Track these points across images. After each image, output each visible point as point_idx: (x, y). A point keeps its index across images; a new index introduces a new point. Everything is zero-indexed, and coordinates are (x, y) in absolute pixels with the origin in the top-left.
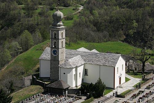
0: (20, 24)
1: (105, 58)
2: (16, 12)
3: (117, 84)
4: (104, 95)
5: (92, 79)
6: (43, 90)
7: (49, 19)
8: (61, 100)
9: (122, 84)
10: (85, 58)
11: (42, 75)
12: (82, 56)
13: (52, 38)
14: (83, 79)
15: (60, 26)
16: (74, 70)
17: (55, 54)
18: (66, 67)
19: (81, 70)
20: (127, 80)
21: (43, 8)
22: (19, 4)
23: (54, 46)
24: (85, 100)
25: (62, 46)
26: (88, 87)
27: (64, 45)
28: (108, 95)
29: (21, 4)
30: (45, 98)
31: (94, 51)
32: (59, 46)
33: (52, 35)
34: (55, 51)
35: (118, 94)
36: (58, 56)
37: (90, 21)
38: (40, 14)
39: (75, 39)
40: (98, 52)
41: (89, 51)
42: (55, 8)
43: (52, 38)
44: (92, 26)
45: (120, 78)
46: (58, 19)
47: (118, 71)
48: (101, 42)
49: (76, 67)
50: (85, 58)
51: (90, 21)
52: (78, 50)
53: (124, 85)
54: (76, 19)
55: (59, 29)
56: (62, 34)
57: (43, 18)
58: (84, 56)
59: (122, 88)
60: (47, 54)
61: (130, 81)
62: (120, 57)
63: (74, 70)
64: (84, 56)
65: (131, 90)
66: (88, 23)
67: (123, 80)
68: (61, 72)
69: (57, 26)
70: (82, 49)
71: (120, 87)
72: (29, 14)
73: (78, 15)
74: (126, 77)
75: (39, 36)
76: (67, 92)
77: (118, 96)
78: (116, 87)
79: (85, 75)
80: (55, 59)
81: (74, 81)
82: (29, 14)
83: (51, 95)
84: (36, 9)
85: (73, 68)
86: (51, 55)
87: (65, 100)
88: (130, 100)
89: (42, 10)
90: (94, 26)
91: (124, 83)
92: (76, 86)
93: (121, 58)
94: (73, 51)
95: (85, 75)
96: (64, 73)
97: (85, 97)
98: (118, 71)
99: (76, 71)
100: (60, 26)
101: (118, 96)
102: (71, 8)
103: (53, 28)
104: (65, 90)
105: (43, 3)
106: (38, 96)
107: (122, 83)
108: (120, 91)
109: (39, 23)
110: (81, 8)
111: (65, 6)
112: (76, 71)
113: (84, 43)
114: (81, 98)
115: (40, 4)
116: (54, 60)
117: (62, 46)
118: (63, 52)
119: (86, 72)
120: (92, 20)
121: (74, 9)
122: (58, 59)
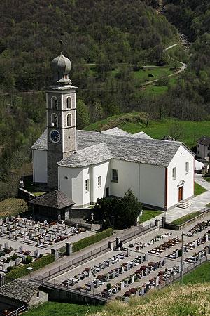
0: (86, 92)
1: (150, 149)
2: (81, 73)
3: (172, 199)
4: (140, 223)
5: (120, 191)
6: (24, 209)
7: (129, 84)
8: (47, 232)
9: (186, 200)
10: (114, 148)
11: (37, 180)
12: (109, 144)
13: (49, 109)
14: (107, 190)
15: (63, 84)
16: (85, 172)
17: (56, 140)
18: (68, 165)
19: (102, 171)
20: (198, 190)
21: (123, 67)
22: (88, 62)
23: (53, 124)
24: (98, 231)
25: (69, 124)
26: (106, 205)
27: (74, 123)
28: (146, 224)
29: (92, 62)
30: (21, 225)
31: (141, 135)
32: (61, 124)
33: (49, 103)
34: (57, 133)
35: (168, 221)
36: (61, 143)
37: (194, 88)
38: (118, 77)
39: (158, 114)
40: (149, 137)
41: (129, 135)
42: (142, 68)
43: (49, 109)
44: (197, 95)
45: (182, 188)
46: (61, 71)
47: (174, 175)
48: (201, 120)
49: (91, 166)
50: (114, 148)
51: (194, 88)
52: (104, 132)
53: (190, 202)
54: (173, 84)
55: (61, 90)
56: (69, 101)
57: (120, 83)
58: (114, 144)
59: (183, 207)
60: (42, 142)
61: (205, 193)
62: (181, 146)
63: (85, 172)
64: (114, 144)
65: (198, 213)
66: (191, 90)
67: (189, 191)
68: (62, 173)
69: (57, 85)
70: (116, 132)
71: (180, 206)
72: (100, 76)
73: (177, 78)
74: (195, 182)
75: (100, 109)
76: (67, 214)
77: (166, 226)
78: (168, 206)
79: (112, 181)
80: (55, 151)
81: (87, 190)
82: (100, 76)
83: (36, 220)
84: (113, 69)
85: (83, 168)
86: (49, 141)
87: (57, 232)
88: (187, 235)
89: (121, 71)
90: (201, 94)
91: (190, 198)
92: (91, 203)
93: (182, 149)
94: (94, 135)
95: (112, 181)
96: (67, 178)
97: (98, 227)
98: (174, 175)
99: (91, 172)
100: (63, 84)
101: (166, 226)
102: (167, 67)
103: (51, 89)
104: (63, 211)
105: (124, 61)
106: (10, 220)
107: (185, 197)
108: (172, 216)
109: (115, 90)
110: (183, 67)
111: (158, 64)
112: (91, 172)
113: (174, 121)
114: (89, 229)
115: (121, 62)
116: (54, 152)
117: (69, 124)
118: (71, 137)
119: (113, 175)
120: (197, 86)
121: (171, 69)
122: (61, 148)
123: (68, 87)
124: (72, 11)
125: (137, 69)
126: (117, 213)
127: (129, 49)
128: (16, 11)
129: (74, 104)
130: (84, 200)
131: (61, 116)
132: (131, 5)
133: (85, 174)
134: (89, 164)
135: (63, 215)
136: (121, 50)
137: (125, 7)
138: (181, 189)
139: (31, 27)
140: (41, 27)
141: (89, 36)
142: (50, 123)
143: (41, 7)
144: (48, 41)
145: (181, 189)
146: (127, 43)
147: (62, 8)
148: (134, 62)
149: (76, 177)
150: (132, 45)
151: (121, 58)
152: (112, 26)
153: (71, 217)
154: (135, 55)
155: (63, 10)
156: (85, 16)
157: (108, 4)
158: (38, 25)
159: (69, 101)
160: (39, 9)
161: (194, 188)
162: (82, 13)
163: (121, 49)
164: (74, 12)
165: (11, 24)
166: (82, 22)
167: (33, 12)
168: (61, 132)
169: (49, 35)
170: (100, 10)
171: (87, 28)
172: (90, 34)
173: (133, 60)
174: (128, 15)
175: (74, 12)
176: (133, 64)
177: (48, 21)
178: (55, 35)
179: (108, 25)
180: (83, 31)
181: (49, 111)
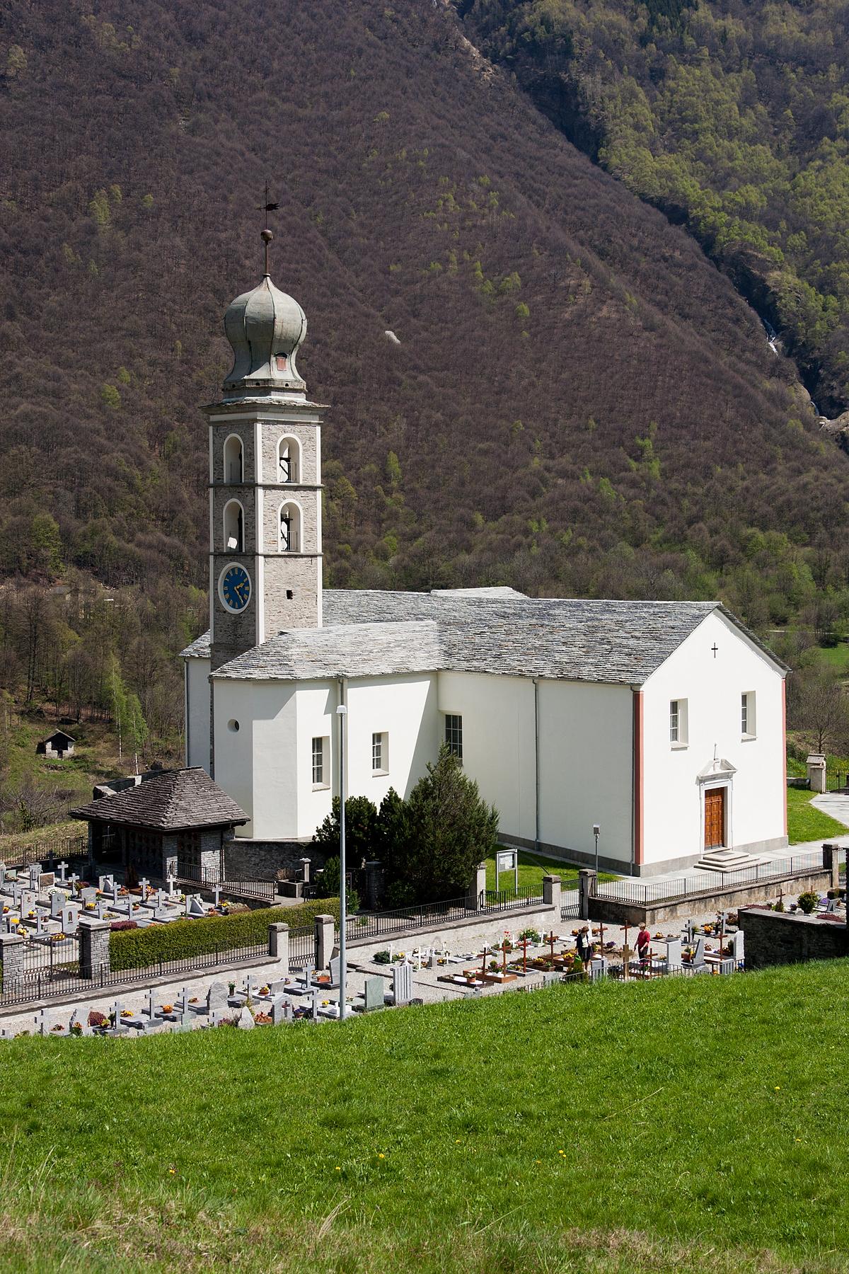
12: (445, 624)
15: (265, 387)
17: (236, 603)
23: (233, 543)
36: (252, 612)
45: (722, 792)
46: (260, 340)
49: (338, 685)
55: (254, 407)
56: (288, 456)
58: (461, 625)
76: (210, 860)
78: (649, 857)
85: (295, 683)
104: (191, 840)
123: (286, 398)
124: (648, 491)
125: (829, 643)
126: (405, 857)
127: (809, 587)
128: (489, 490)
129: (311, 467)
130: (304, 815)
131: (253, 507)
132: (824, 475)
133: (310, 713)
134: (331, 673)
135: (190, 868)
136: (783, 590)
137: (806, 478)
138: (717, 799)
139: (527, 532)
140: (552, 531)
141: (691, 554)
142: (219, 540)
143: (560, 481)
144: (569, 566)
145: (717, 799)
146: (802, 574)
147: (620, 482)
148: (820, 622)
149: (270, 715)
150: (819, 579)
151: (782, 610)
152: (764, 528)
153: (230, 869)
154: (826, 602)
155: (621, 488)
156: (686, 502)
157: (756, 473)
158: (545, 526)
159: (288, 456)
160: (555, 485)
161: (834, 821)
162: (677, 496)
163: (785, 585)
164: (653, 493)
165: (471, 525)
166: (673, 518)
167: (534, 494)
168: (253, 569)
169: (573, 552)
170: (731, 489)
171: (689, 532)
172: (696, 548)
173: (819, 618)
174: (815, 498)
175: (653, 493)
176: (818, 627)
177: (575, 514)
178: (592, 550)
179: (752, 525)
180: (678, 540)
181: (215, 494)
